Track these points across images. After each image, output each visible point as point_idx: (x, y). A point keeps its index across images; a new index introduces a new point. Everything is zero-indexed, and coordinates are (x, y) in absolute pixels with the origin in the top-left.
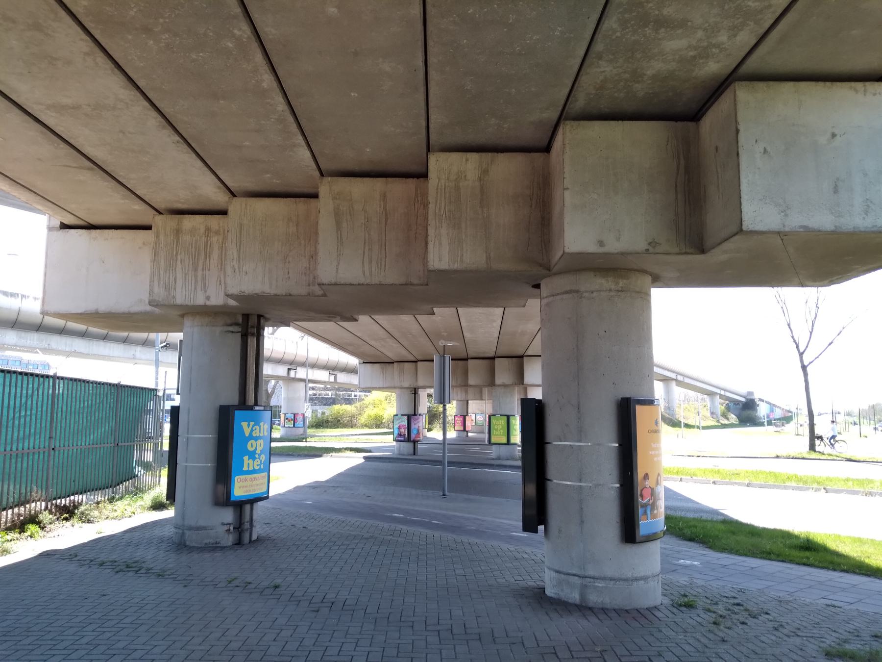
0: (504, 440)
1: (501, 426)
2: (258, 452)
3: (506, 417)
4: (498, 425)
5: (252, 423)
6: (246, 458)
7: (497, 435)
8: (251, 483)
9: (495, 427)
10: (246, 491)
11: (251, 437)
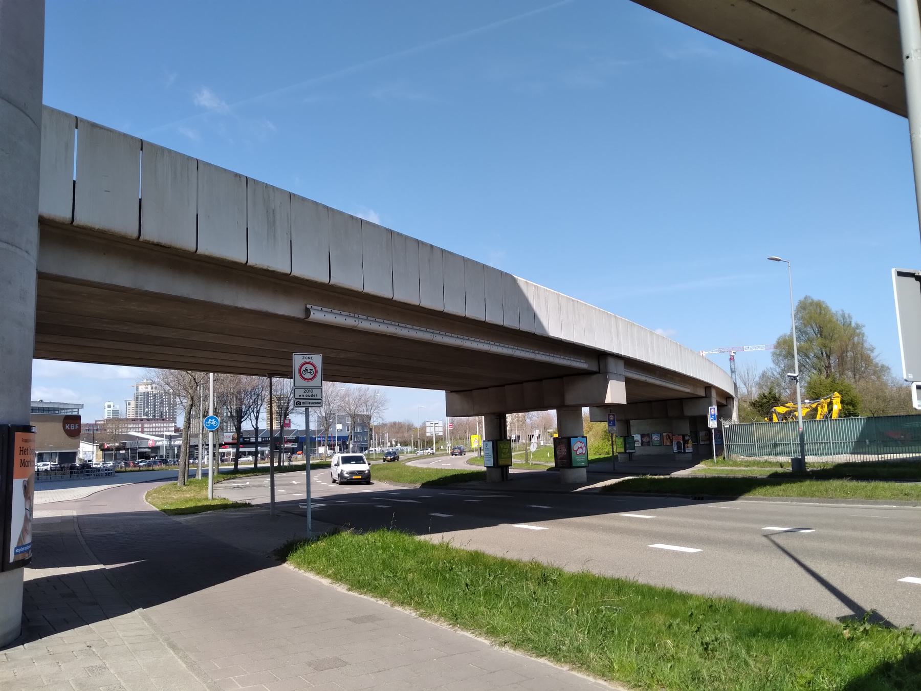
11: (503, 448)
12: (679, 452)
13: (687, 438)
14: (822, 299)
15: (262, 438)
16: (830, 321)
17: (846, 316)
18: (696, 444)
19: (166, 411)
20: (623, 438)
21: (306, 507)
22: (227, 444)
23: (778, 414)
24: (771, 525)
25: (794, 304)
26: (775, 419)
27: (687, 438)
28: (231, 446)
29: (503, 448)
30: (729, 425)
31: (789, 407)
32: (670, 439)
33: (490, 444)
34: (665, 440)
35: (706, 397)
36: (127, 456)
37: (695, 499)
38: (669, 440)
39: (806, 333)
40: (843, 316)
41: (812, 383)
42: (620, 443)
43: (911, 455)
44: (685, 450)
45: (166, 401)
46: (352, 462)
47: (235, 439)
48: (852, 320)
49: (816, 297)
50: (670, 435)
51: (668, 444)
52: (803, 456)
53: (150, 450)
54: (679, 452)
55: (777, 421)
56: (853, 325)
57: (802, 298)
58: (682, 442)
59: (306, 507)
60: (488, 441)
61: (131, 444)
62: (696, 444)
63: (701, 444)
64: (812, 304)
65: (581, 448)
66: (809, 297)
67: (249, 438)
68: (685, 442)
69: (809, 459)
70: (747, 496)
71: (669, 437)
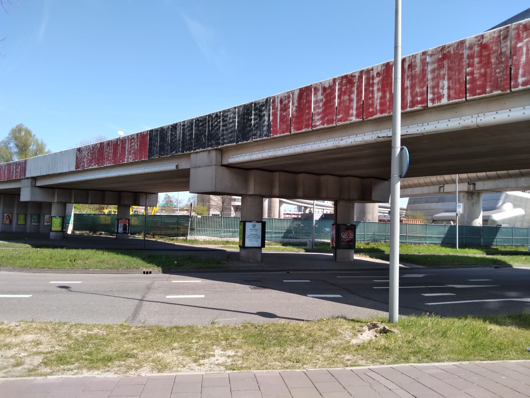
12: (124, 233)
18: (38, 224)
20: (62, 218)
21: (388, 263)
24: (173, 294)
30: (202, 216)
32: (10, 219)
34: (5, 218)
38: (8, 219)
40: (42, 143)
42: (58, 222)
48: (46, 148)
50: (10, 215)
51: (8, 222)
54: (124, 233)
55: (267, 217)
58: (127, 225)
59: (388, 263)
60: (257, 222)
62: (38, 224)
63: (45, 224)
71: (9, 218)
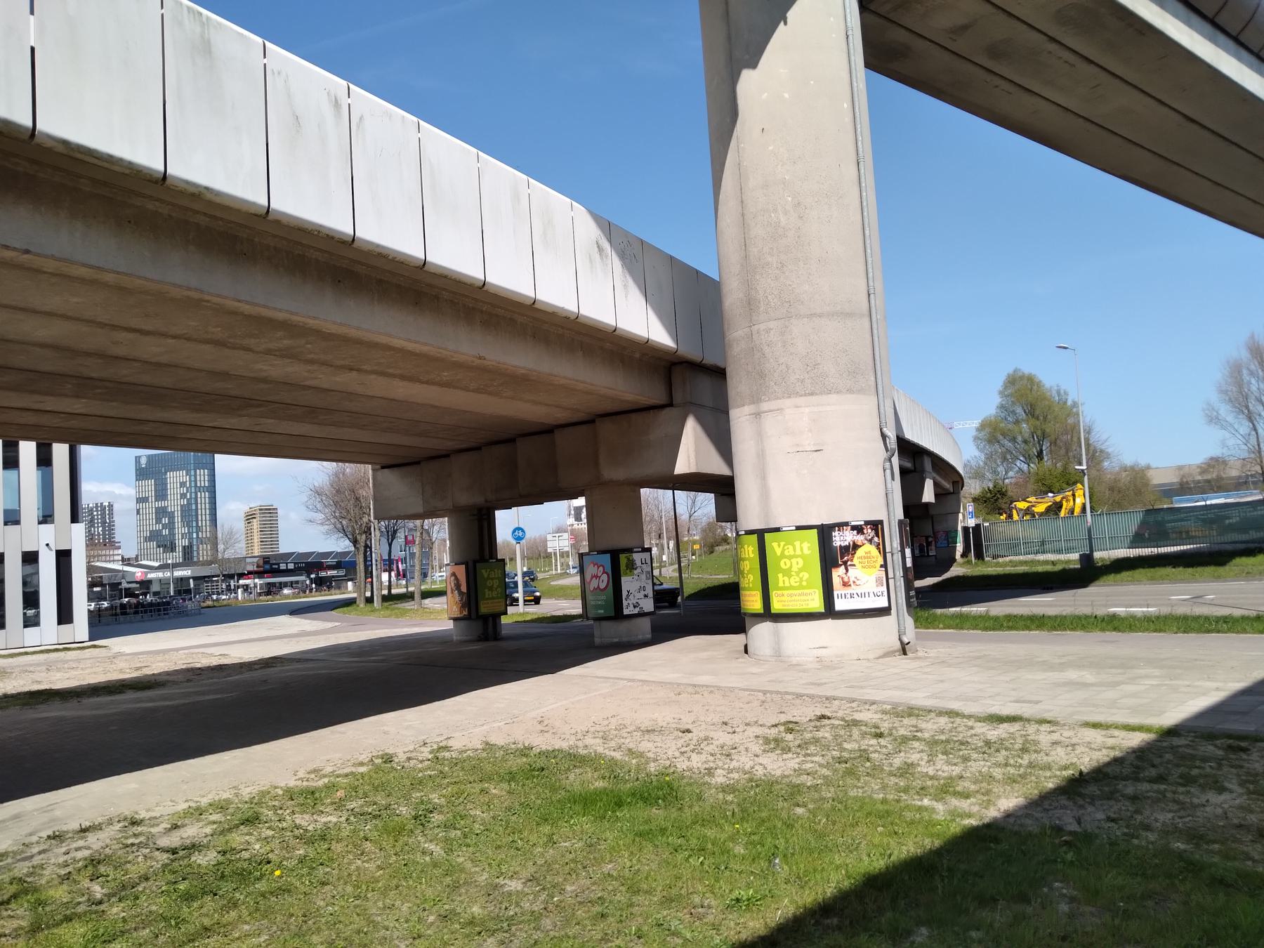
0: (817, 604)
1: (801, 561)
2: (495, 586)
3: (609, 555)
4: (790, 558)
5: (782, 544)
6: (780, 575)
7: (791, 588)
8: (789, 598)
9: (782, 564)
10: (783, 606)
11: (488, 578)
13: (930, 539)
14: (1033, 373)
15: (295, 563)
16: (1045, 399)
17: (1062, 392)
19: (99, 533)
22: (250, 573)
23: (1018, 510)
25: (999, 382)
26: (1016, 517)
27: (930, 539)
28: (256, 575)
29: (783, 556)
31: (1031, 502)
33: (461, 571)
35: (953, 493)
36: (104, 595)
37: (1044, 589)
39: (1014, 412)
40: (1059, 393)
41: (1041, 473)
43: (1189, 547)
44: (928, 553)
45: (98, 519)
46: (908, 551)
47: (261, 567)
49: (1027, 369)
52: (1092, 551)
53: (138, 585)
54: (922, 556)
56: (1069, 403)
57: (1011, 371)
61: (110, 578)
64: (1022, 378)
65: (596, 577)
66: (1020, 370)
67: (278, 564)
68: (929, 544)
69: (1097, 555)
70: (1097, 583)
